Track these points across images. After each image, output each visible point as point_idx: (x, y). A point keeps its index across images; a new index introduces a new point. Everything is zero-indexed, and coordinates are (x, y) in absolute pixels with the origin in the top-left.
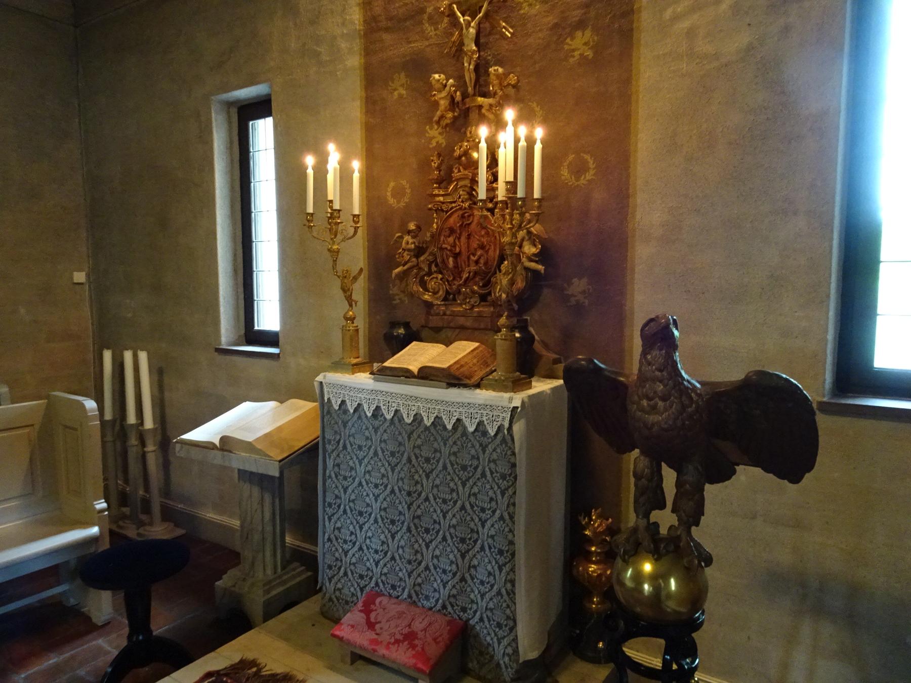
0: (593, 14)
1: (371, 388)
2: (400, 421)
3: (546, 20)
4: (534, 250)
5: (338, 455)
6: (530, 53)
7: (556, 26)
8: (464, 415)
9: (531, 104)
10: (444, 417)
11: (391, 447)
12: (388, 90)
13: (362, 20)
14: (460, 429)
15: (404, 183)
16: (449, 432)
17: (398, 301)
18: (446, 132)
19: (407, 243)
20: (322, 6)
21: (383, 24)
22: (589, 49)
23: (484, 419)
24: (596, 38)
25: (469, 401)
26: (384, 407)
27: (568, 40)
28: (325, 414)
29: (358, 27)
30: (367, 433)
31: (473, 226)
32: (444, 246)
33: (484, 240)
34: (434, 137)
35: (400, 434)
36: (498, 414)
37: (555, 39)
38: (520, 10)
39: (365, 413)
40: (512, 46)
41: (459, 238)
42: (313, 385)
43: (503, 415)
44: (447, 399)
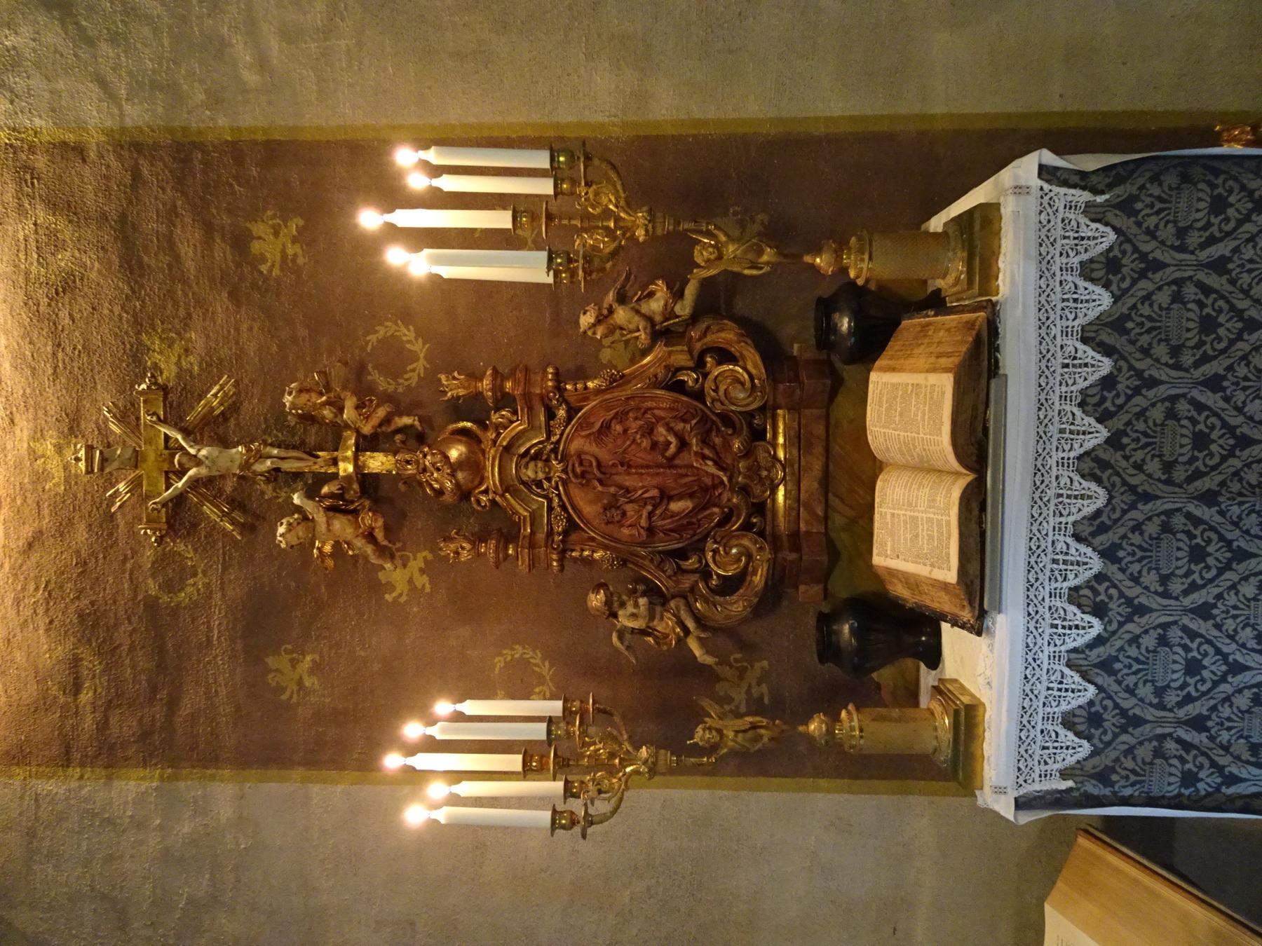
0: (226, 220)
1: (1021, 618)
2: (1103, 529)
3: (221, 316)
4: (660, 287)
5: (1226, 748)
6: (275, 348)
7: (234, 295)
8: (1070, 323)
9: (370, 347)
10: (1082, 384)
11: (1174, 556)
12: (298, 704)
13: (141, 772)
14: (1104, 337)
15: (499, 662)
16: (1120, 370)
17: (764, 688)
18: (403, 549)
19: (634, 616)
20: (93, 889)
21: (159, 711)
22: (286, 226)
23: (1075, 261)
24: (269, 213)
25: (1033, 310)
26: (1071, 576)
27: (264, 268)
28: (1107, 791)
29: (155, 784)
30: (1149, 641)
31: (604, 455)
32: (643, 523)
33: (634, 425)
34: (410, 581)
35: (1137, 528)
36: (1060, 225)
37: (257, 296)
38: (191, 372)
39: (1092, 645)
40: (255, 391)
41: (628, 491)
42: (1027, 825)
43: (1061, 209)
44: (1034, 369)
